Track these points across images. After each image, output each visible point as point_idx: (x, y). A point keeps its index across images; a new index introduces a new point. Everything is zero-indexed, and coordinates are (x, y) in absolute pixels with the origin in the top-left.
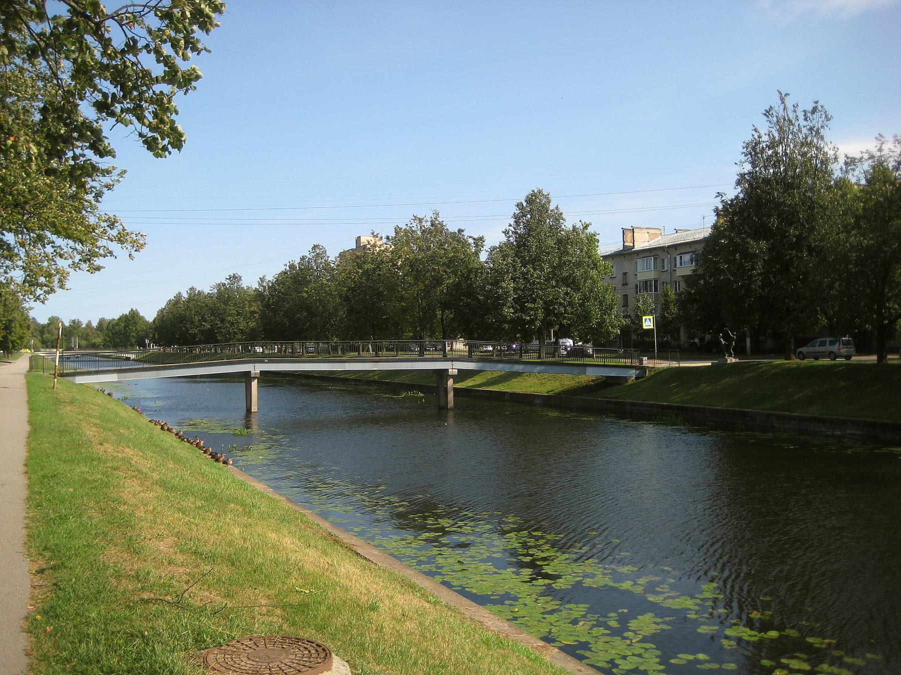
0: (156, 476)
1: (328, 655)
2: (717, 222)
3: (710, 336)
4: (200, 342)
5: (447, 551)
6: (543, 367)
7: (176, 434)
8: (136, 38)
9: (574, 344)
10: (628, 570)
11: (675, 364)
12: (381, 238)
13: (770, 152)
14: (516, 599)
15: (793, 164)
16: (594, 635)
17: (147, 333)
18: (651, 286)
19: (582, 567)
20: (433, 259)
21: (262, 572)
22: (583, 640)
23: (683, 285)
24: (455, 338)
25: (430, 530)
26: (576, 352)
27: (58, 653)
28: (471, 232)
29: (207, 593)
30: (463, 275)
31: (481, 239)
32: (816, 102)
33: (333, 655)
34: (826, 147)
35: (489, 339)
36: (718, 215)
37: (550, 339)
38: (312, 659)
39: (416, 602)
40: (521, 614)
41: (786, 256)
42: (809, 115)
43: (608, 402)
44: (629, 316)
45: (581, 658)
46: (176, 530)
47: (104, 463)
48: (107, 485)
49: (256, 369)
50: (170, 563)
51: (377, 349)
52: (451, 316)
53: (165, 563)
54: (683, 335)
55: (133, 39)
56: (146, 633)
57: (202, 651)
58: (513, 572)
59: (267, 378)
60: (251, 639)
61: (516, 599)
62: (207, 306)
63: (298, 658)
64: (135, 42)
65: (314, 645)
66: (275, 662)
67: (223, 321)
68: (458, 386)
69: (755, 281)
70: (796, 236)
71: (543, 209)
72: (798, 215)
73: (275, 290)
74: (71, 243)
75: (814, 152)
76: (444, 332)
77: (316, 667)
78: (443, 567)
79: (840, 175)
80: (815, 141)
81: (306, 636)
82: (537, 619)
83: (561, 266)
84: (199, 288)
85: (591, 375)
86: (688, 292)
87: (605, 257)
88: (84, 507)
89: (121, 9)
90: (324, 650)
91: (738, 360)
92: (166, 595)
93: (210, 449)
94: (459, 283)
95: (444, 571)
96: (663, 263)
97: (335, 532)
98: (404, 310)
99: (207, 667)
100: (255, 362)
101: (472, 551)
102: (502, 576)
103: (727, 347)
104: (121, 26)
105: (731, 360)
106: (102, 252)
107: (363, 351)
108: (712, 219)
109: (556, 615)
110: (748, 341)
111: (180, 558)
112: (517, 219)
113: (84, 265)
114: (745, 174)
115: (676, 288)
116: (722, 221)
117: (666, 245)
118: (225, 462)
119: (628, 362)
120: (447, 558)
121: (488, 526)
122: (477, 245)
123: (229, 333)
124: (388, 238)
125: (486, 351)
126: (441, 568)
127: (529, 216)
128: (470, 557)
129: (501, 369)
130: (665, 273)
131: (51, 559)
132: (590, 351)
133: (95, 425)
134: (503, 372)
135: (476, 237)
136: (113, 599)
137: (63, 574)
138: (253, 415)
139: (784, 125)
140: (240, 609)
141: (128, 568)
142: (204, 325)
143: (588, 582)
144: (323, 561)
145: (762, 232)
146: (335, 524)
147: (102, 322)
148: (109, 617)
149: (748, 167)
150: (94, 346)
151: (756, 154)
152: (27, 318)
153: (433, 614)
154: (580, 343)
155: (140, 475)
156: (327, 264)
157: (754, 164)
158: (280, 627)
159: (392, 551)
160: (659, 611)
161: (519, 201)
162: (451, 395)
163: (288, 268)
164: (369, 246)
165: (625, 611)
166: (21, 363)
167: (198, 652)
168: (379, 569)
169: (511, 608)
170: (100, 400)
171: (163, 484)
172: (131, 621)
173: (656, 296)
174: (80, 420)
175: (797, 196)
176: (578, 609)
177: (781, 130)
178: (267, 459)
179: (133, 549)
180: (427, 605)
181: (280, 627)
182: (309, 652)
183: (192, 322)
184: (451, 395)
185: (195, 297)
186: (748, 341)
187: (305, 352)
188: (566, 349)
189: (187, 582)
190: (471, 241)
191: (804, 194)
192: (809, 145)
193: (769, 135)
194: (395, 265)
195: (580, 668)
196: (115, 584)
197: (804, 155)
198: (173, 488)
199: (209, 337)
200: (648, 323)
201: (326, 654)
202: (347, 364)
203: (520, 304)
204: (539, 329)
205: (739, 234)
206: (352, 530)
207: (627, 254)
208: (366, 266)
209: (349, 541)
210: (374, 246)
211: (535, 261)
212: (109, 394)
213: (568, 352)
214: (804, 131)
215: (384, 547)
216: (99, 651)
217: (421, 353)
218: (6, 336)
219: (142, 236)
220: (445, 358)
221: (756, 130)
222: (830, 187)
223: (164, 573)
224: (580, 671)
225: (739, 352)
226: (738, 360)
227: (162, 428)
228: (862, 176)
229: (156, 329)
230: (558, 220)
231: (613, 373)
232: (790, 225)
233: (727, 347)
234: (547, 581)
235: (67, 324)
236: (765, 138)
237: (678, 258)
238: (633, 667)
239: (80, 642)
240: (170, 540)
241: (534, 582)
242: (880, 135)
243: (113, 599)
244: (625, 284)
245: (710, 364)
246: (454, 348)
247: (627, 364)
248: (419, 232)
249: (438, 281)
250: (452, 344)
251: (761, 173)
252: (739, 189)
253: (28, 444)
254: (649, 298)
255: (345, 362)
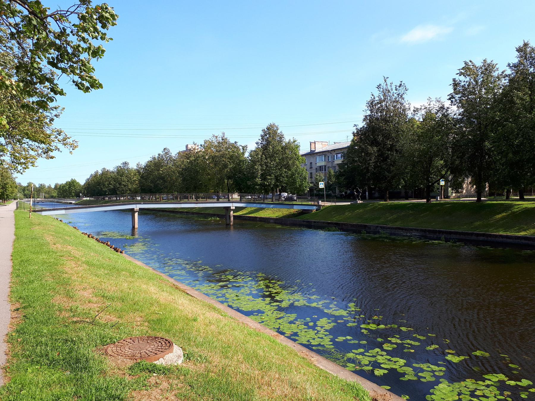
0: (84, 259)
1: (171, 344)
2: (354, 139)
3: (349, 191)
4: (108, 195)
5: (230, 291)
6: (274, 205)
7: (96, 239)
8: (66, 28)
9: (288, 195)
10: (315, 298)
11: (334, 204)
12: (198, 145)
13: (379, 105)
14: (263, 313)
15: (390, 111)
16: (300, 329)
17: (81, 190)
18: (323, 168)
19: (293, 297)
20: (223, 156)
21: (138, 305)
22: (295, 331)
23: (337, 168)
24: (233, 193)
25: (223, 281)
26: (288, 199)
27: (24, 352)
28: (241, 143)
29: (108, 316)
30: (237, 164)
31: (246, 146)
32: (401, 82)
33: (174, 344)
34: (405, 103)
35: (249, 193)
36: (354, 135)
37: (277, 193)
38: (163, 347)
39: (216, 316)
40: (266, 319)
41: (386, 154)
42: (398, 87)
43: (303, 221)
44: (313, 182)
45: (295, 340)
46: (94, 285)
47: (56, 253)
48: (56, 265)
49: (137, 207)
50: (89, 302)
51: (197, 198)
52: (232, 183)
53: (87, 302)
54: (337, 191)
55: (63, 28)
56: (74, 339)
57: (105, 346)
58: (261, 300)
59: (142, 212)
60: (131, 339)
61: (263, 313)
62: (111, 177)
63: (156, 347)
64: (65, 30)
65: (164, 340)
66: (144, 350)
67: (120, 184)
68: (235, 214)
69: (371, 165)
70: (390, 145)
71: (275, 132)
72: (391, 135)
73: (146, 170)
74: (37, 144)
75: (399, 106)
76: (229, 190)
77: (165, 351)
78: (229, 298)
79: (411, 116)
80: (400, 100)
81: (160, 336)
82: (273, 322)
83: (283, 159)
84: (107, 168)
85: (296, 209)
86: (340, 171)
87: (302, 155)
88: (43, 275)
89: (55, 12)
90: (169, 342)
91: (362, 202)
92: (86, 318)
93: (113, 246)
94: (235, 167)
95: (228, 300)
96: (329, 158)
97: (176, 284)
98: (210, 180)
99: (107, 355)
100: (136, 204)
101: (242, 290)
102: (257, 302)
103: (358, 196)
104: (56, 21)
105: (359, 202)
106: (53, 148)
107: (190, 199)
108: (351, 137)
109: (282, 319)
110: (367, 193)
111: (95, 299)
112: (262, 137)
113: (44, 155)
114: (367, 116)
115: (334, 169)
116: (356, 138)
117: (330, 150)
118: (121, 252)
119: (313, 203)
120: (230, 294)
121: (250, 278)
122: (243, 150)
123: (123, 190)
124: (201, 145)
125: (248, 199)
126: (228, 299)
127: (268, 136)
128: (242, 293)
129: (254, 206)
130: (329, 163)
131: (23, 303)
132: (295, 198)
133: (52, 235)
134: (256, 208)
135: (243, 146)
136: (57, 322)
137: (30, 310)
138: (136, 229)
139: (386, 93)
140: (126, 324)
141: (66, 306)
142: (110, 187)
143: (296, 304)
144: (170, 298)
145: (374, 143)
146: (176, 280)
147: (56, 186)
148: (54, 332)
149: (369, 113)
150: (52, 197)
151: (373, 106)
152: (15, 183)
153: (225, 321)
154: (291, 195)
155: (76, 259)
156: (171, 157)
157: (371, 111)
158: (147, 332)
159: (204, 292)
160: (328, 316)
161: (263, 129)
162: (232, 219)
163: (152, 159)
164: (192, 149)
165: (316, 316)
166: (12, 205)
167: (103, 347)
168: (198, 300)
169: (261, 317)
170: (56, 223)
171: (87, 263)
172: (66, 333)
173: (325, 173)
174: (43, 233)
175: (392, 126)
176: (292, 316)
177: (384, 95)
178: (143, 250)
179: (69, 296)
180: (221, 317)
181: (147, 332)
182: (162, 343)
183: (104, 185)
184: (232, 219)
185: (105, 173)
186: (367, 193)
187: (161, 199)
188: (284, 197)
189: (98, 311)
190: (241, 148)
191: (394, 125)
192: (397, 102)
193: (379, 97)
194: (204, 158)
195: (294, 345)
196: (58, 314)
197: (395, 107)
198: (93, 265)
199: (114, 192)
200: (322, 185)
201: (170, 344)
202: (182, 204)
203: (264, 177)
204: (272, 188)
205: (364, 144)
206: (185, 283)
207: (312, 154)
208: (191, 159)
209: (183, 288)
210: (194, 149)
211: (272, 157)
212: (61, 221)
213: (285, 199)
214: (395, 95)
215: (201, 290)
216: (47, 350)
217: (218, 199)
218: (3, 192)
219: (76, 142)
220: (229, 202)
221: (373, 95)
222: (406, 122)
223: (87, 307)
224: (294, 346)
225: (363, 198)
226: (362, 202)
227: (89, 237)
228: (421, 117)
229: (85, 188)
230: (281, 138)
231: (306, 208)
232: (388, 139)
233: (358, 196)
234: (278, 304)
235: (37, 186)
236: (377, 99)
237: (335, 155)
238: (318, 343)
239: (37, 345)
240: (90, 291)
241: (272, 304)
242: (430, 98)
243: (57, 322)
244: (311, 168)
245: (350, 204)
246: (233, 197)
247: (312, 204)
248: (216, 143)
249: (225, 166)
250: (232, 195)
251: (375, 115)
252: (365, 123)
253: (14, 245)
254: (322, 175)
255: (181, 204)
